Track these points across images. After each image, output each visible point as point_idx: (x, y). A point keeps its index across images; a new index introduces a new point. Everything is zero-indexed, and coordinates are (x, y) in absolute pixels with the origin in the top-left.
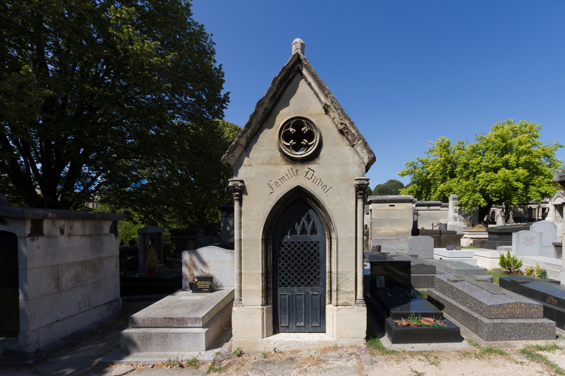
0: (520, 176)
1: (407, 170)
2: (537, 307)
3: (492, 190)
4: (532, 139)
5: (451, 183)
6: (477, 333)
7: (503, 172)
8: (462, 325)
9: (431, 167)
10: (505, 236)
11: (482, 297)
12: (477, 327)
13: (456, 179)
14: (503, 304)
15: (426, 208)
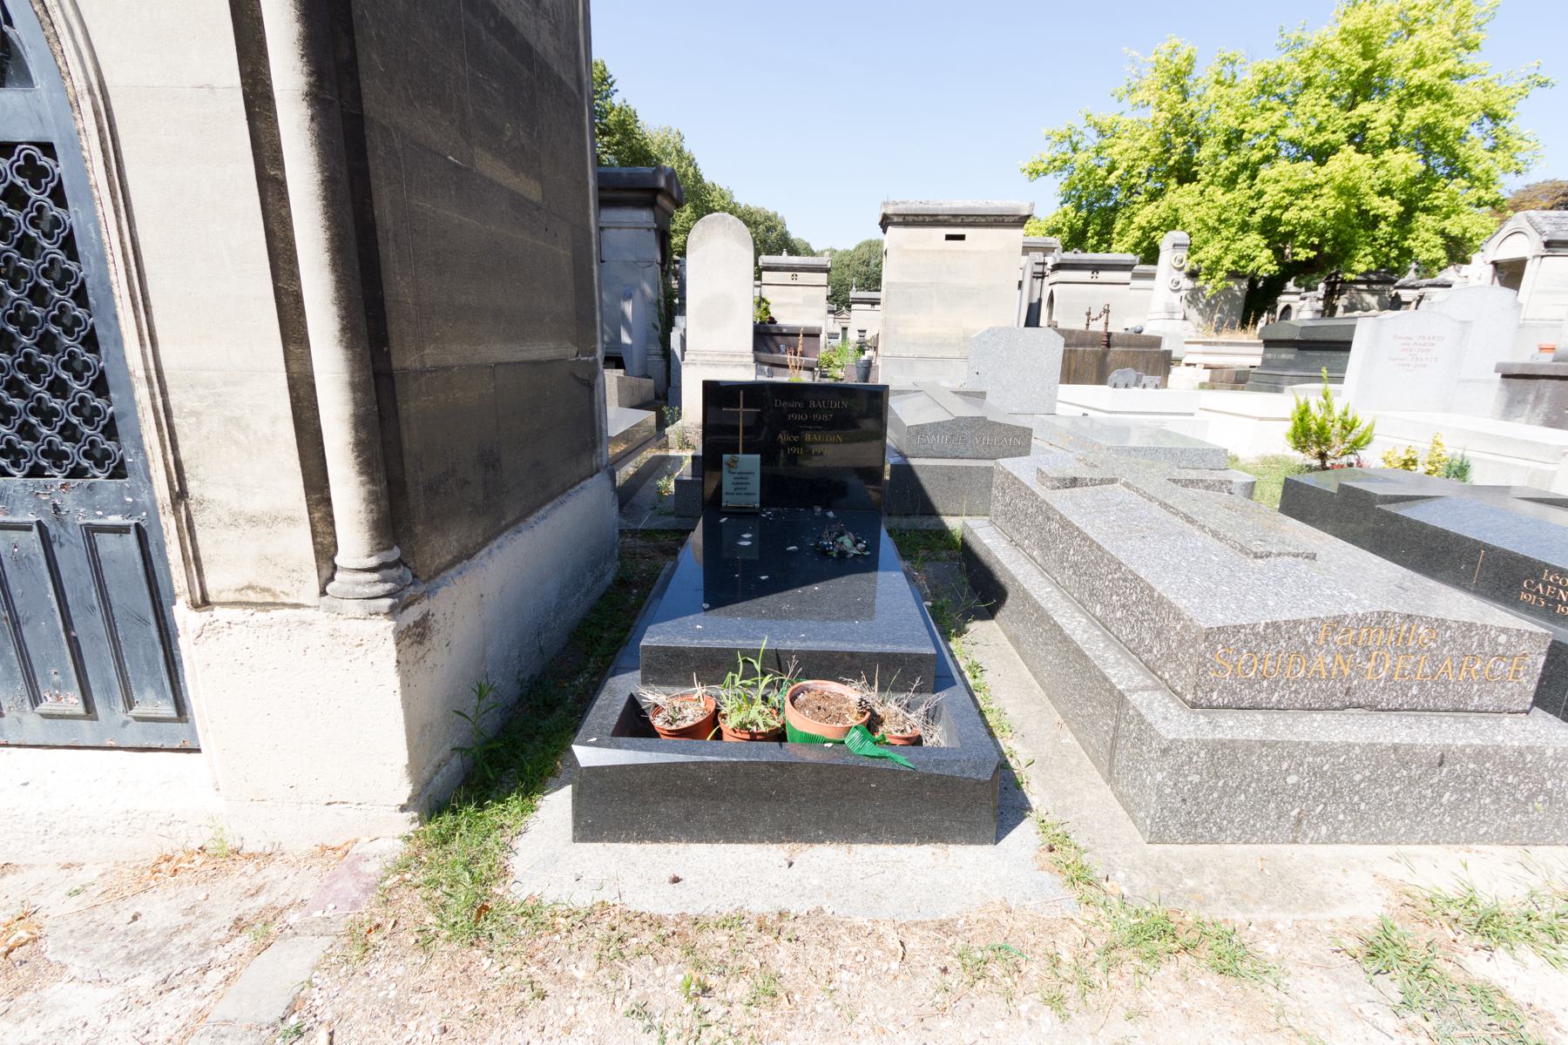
0: (1395, 175)
1: (1048, 156)
2: (1509, 645)
3: (1298, 223)
4: (1458, 55)
5: (1180, 197)
6: (1110, 778)
7: (1346, 162)
8: (1052, 709)
9: (1124, 144)
10: (1317, 354)
11: (1176, 569)
12: (1113, 747)
13: (1194, 187)
14: (1297, 623)
15: (1086, 275)
